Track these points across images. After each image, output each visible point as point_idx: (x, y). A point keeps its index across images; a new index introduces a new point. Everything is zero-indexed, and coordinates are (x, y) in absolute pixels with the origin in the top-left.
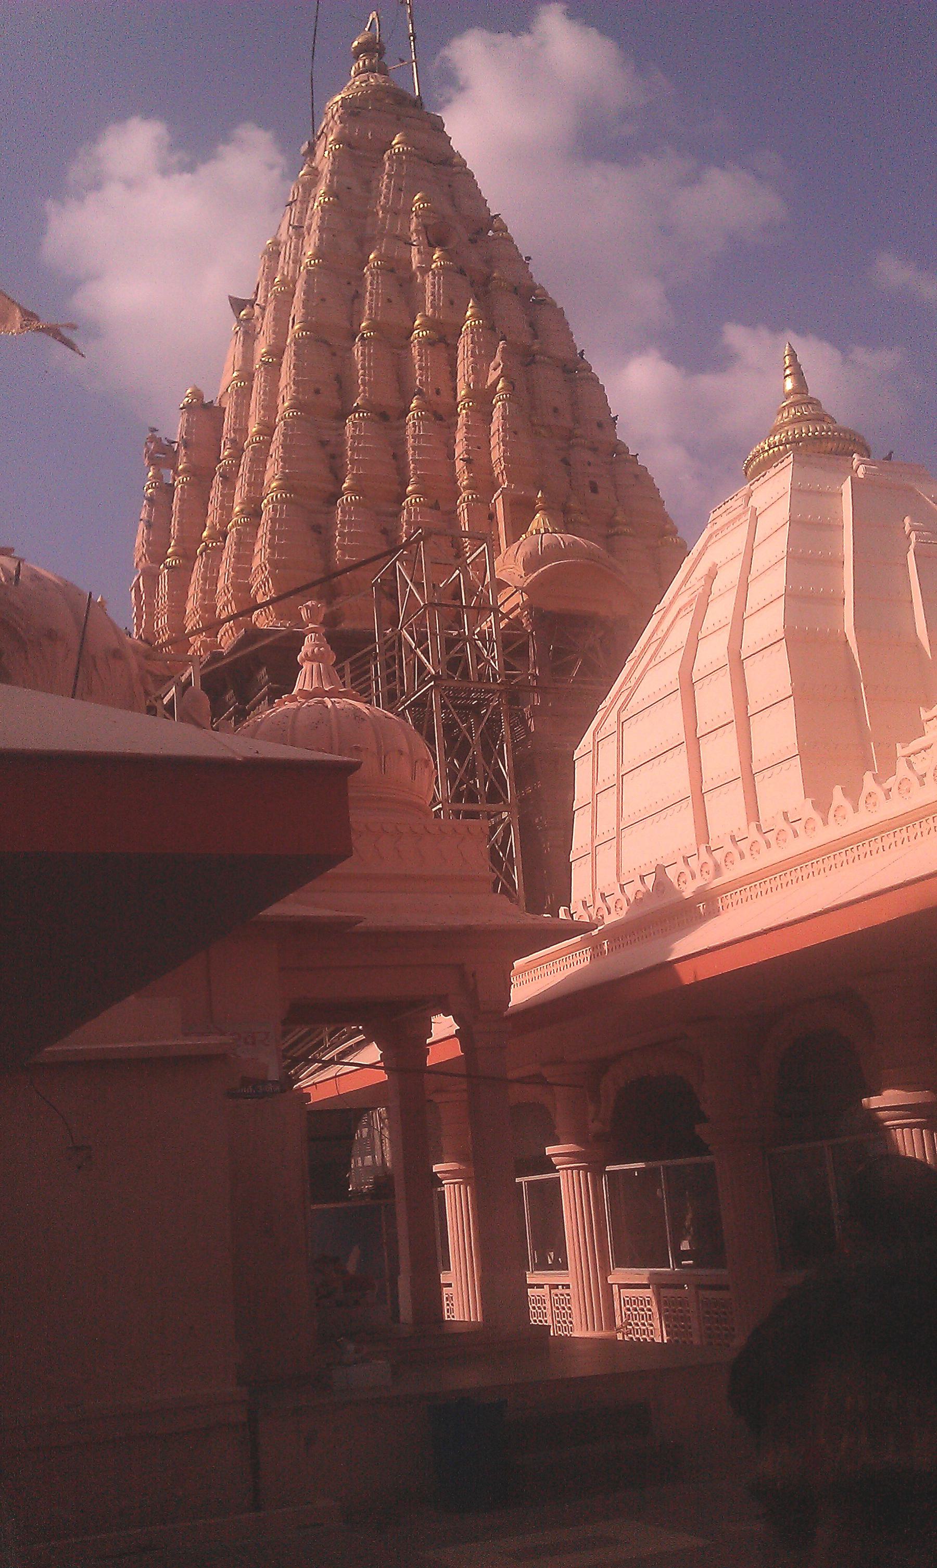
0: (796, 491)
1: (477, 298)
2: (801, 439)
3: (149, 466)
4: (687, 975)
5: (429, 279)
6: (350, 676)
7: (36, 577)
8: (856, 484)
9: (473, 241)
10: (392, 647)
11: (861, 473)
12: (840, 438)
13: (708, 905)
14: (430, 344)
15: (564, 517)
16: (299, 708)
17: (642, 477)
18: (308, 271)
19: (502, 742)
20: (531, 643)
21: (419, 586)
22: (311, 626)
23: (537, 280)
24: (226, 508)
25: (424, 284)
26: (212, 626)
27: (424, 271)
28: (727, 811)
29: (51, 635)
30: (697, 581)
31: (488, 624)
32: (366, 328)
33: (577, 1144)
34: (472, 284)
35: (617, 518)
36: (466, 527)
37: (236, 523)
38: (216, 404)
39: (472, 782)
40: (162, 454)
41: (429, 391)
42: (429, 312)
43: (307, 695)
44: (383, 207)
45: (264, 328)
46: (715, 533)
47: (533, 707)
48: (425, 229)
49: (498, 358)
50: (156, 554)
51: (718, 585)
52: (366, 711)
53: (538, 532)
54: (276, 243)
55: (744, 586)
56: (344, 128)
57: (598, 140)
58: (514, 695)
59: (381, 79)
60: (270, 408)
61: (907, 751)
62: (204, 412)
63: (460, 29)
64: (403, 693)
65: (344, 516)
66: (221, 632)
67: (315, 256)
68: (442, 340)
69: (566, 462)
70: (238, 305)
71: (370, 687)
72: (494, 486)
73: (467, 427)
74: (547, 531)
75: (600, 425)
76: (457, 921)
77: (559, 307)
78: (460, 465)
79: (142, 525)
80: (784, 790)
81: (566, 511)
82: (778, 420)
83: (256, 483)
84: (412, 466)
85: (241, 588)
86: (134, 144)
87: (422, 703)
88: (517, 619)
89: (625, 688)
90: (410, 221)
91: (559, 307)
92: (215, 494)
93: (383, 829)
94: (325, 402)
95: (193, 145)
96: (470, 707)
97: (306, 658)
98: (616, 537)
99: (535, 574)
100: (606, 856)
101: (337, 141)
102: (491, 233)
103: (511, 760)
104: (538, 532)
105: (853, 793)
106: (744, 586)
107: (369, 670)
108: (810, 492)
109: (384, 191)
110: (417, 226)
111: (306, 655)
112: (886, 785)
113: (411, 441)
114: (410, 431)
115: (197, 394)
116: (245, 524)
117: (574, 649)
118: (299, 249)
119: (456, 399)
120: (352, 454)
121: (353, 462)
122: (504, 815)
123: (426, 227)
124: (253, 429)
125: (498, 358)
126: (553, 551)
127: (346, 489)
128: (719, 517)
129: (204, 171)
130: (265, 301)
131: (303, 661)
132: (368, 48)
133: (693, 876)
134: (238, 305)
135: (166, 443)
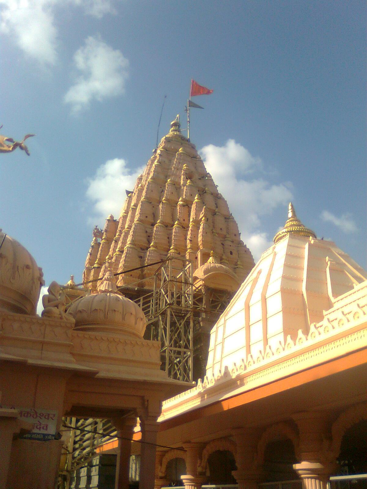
0: (289, 245)
1: (200, 195)
2: (292, 231)
3: (94, 237)
5: (185, 188)
8: (310, 245)
11: (312, 242)
12: (306, 232)
14: (183, 206)
15: (220, 260)
18: (148, 183)
19: (190, 328)
20: (204, 298)
22: (109, 269)
24: (114, 250)
25: (184, 189)
27: (184, 185)
28: (256, 349)
32: (164, 200)
33: (192, 475)
35: (238, 263)
37: (116, 254)
40: (98, 233)
42: (184, 197)
43: (102, 292)
44: (174, 167)
48: (186, 174)
49: (203, 211)
50: (91, 262)
52: (121, 298)
53: (210, 263)
54: (142, 176)
55: (269, 275)
56: (165, 145)
58: (197, 314)
59: (178, 133)
60: (132, 221)
62: (112, 222)
64: (159, 310)
65: (149, 253)
67: (151, 179)
68: (187, 205)
73: (191, 230)
75: (235, 235)
78: (188, 241)
84: (173, 241)
92: (112, 246)
96: (181, 316)
99: (207, 275)
102: (207, 178)
103: (193, 334)
104: (210, 263)
106: (269, 275)
108: (294, 246)
110: (183, 173)
111: (105, 279)
113: (174, 234)
114: (174, 231)
115: (112, 217)
116: (119, 255)
117: (216, 299)
118: (147, 177)
121: (155, 238)
124: (126, 227)
125: (203, 211)
126: (214, 268)
127: (151, 246)
132: (175, 125)
133: (237, 370)
134: (128, 192)
135: (100, 230)
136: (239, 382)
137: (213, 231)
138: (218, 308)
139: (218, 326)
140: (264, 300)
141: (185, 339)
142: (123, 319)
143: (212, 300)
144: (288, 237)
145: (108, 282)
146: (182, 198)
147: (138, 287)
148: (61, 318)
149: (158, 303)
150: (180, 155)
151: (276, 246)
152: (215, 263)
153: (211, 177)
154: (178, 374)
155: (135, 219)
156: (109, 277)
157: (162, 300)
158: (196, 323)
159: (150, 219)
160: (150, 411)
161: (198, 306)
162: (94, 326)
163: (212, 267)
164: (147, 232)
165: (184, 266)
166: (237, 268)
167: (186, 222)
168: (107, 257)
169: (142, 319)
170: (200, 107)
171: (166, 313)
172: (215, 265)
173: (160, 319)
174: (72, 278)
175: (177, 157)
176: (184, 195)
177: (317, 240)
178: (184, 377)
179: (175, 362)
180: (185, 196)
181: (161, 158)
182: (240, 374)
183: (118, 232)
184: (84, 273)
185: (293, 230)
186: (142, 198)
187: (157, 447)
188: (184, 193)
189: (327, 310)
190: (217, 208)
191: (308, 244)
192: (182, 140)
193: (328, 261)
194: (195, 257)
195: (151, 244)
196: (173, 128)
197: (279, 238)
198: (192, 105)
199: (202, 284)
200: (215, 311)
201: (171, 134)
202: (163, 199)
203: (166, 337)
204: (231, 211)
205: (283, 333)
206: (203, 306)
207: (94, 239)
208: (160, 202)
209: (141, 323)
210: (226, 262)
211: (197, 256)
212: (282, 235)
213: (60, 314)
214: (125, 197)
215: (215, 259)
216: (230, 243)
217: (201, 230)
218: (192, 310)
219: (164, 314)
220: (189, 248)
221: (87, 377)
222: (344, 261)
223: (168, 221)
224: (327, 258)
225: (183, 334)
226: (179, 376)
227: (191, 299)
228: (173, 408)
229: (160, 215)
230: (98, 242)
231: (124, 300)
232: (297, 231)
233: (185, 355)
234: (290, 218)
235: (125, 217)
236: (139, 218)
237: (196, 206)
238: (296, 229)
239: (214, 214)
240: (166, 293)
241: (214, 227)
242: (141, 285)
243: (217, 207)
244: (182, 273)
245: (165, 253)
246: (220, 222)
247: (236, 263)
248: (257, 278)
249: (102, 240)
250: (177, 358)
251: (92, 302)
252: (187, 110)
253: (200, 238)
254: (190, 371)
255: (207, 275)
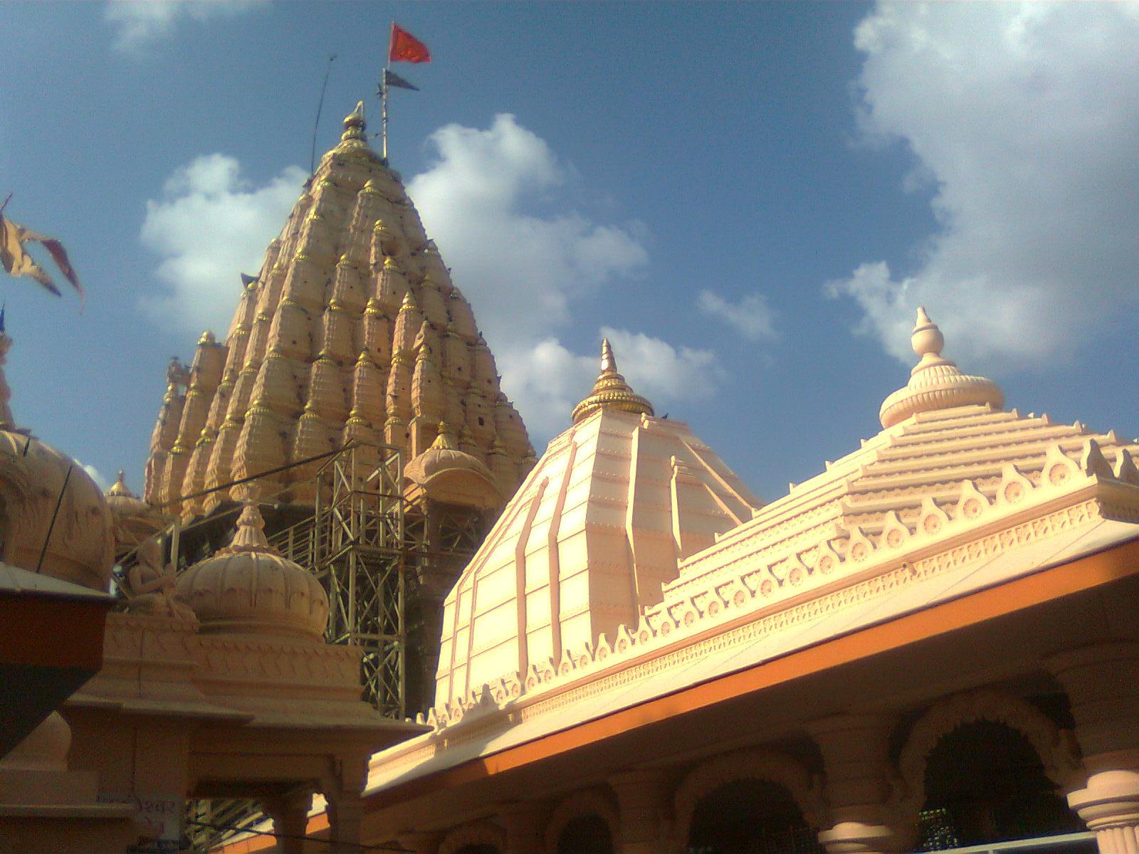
2: (609, 401)
4: (492, 768)
5: (380, 276)
6: (293, 538)
7: (41, 452)
8: (641, 431)
9: (413, 254)
10: (326, 520)
12: (634, 402)
13: (515, 715)
15: (458, 439)
16: (230, 558)
17: (514, 417)
18: (297, 263)
21: (348, 477)
23: (455, 284)
24: (220, 416)
25: (376, 279)
26: (200, 495)
27: (378, 271)
28: (540, 650)
29: (45, 494)
30: (534, 489)
31: (396, 508)
34: (410, 282)
36: (389, 441)
37: (226, 427)
38: (224, 345)
39: (376, 618)
40: (179, 375)
41: (374, 349)
43: (239, 549)
45: (263, 296)
46: (547, 460)
47: (423, 568)
50: (166, 443)
51: (547, 492)
52: (280, 563)
53: (438, 448)
54: (278, 242)
55: (564, 493)
57: (530, 202)
58: (410, 559)
60: (260, 350)
61: (648, 612)
63: (444, 122)
64: (330, 553)
65: (303, 426)
66: (206, 501)
67: (302, 253)
69: (463, 403)
70: (247, 280)
71: (308, 546)
72: (411, 415)
73: (396, 374)
74: (444, 448)
75: (489, 382)
76: (330, 722)
77: (468, 302)
78: (389, 399)
79: (158, 423)
80: (578, 632)
81: (460, 435)
82: (596, 387)
83: (244, 401)
84: (356, 397)
85: (224, 470)
86: (215, 171)
87: (342, 562)
88: (418, 506)
89: (482, 557)
90: (371, 238)
91: (468, 302)
93: (305, 652)
94: (299, 350)
95: (255, 176)
96: (378, 565)
97: (243, 523)
98: (494, 456)
99: (432, 476)
100: (460, 676)
101: (326, 180)
102: (426, 251)
104: (438, 448)
105: (611, 639)
106: (564, 493)
107: (308, 535)
108: (611, 435)
109: (356, 215)
112: (359, 640)
113: (357, 381)
114: (357, 374)
115: (210, 337)
116: (232, 428)
117: (456, 528)
118: (293, 247)
119: (391, 354)
120: (314, 386)
121: (314, 392)
122: (396, 643)
123: (382, 243)
124: (247, 364)
125: (422, 332)
126: (447, 461)
128: (553, 446)
129: (261, 194)
130: (266, 279)
131: (241, 525)
132: (354, 124)
133: (507, 694)
134: (247, 280)
136: (511, 716)
137: (444, 373)
138: (455, 545)
139: (462, 591)
140: (554, 546)
141: (388, 614)
142: (288, 605)
143: (443, 529)
144: (600, 413)
145: (248, 528)
146: (375, 300)
147: (280, 503)
148: (170, 614)
149: (328, 538)
150: (367, 197)
151: (576, 429)
152: (450, 449)
153: (436, 249)
154: (372, 687)
155: (268, 346)
156: (251, 517)
157: (335, 532)
158: (411, 577)
159: (303, 348)
160: (343, 779)
161: (413, 542)
162: (229, 623)
163: (443, 458)
164: (295, 377)
165: (383, 460)
166: (494, 453)
167: (384, 354)
168: (203, 432)
169: (322, 603)
170: (412, 88)
171: (347, 561)
172: (449, 452)
173: (333, 572)
174: (121, 478)
175: (359, 201)
176: (378, 293)
177: (655, 420)
178: (386, 692)
179: (365, 660)
180: (381, 294)
181: (323, 205)
182: (512, 702)
183: (228, 374)
184: (150, 465)
185: (611, 398)
186: (284, 299)
187: (306, 841)
188: (379, 288)
189: (668, 583)
190: (451, 321)
191: (637, 430)
192: (371, 163)
193: (675, 465)
194: (403, 434)
195: (306, 404)
196: (349, 133)
197: (579, 416)
198: (393, 80)
199: (422, 494)
200: (448, 550)
201: (345, 145)
202: (332, 301)
203: (347, 617)
204: (457, 280)
205: (588, 571)
206: (424, 542)
207: (170, 388)
208: (324, 308)
209: (321, 610)
210: (471, 441)
211: (409, 431)
212: (590, 407)
213: (168, 605)
214: (242, 292)
215: (449, 437)
216: (478, 400)
217: (417, 375)
218: (401, 553)
219: (342, 562)
220: (393, 415)
221: (233, 728)
222: (704, 464)
223: (344, 351)
224: (673, 458)
225: (382, 605)
226: (373, 690)
227: (399, 528)
228: (388, 768)
229: (325, 339)
230: (180, 394)
231: (286, 567)
232: (617, 400)
233: (387, 648)
234: (603, 372)
235: (242, 340)
236: (277, 346)
237: (406, 319)
238: (615, 398)
239: (444, 336)
240: (346, 517)
241: (444, 365)
242: (286, 498)
243: (450, 320)
244: (377, 472)
245: (338, 425)
246: (457, 352)
247: (497, 448)
248: (540, 496)
249: (189, 389)
250: (368, 653)
251: (224, 569)
252: (381, 94)
253: (415, 394)
254: (398, 682)
255: (432, 476)
